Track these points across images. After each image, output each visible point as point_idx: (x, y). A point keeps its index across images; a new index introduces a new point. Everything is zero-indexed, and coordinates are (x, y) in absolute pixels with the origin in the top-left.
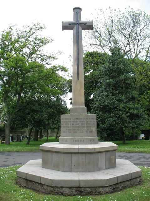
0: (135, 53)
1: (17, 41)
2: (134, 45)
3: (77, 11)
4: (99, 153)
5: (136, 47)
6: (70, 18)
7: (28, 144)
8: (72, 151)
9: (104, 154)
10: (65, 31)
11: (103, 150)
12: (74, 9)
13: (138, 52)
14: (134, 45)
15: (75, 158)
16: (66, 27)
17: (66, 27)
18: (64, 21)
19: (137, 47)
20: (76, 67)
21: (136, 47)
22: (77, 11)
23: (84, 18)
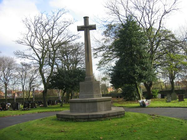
0: (149, 23)
1: (47, 24)
2: (149, 17)
3: (86, 19)
4: (101, 103)
5: (150, 19)
6: (82, 24)
7: (61, 106)
8: (85, 101)
9: (104, 102)
10: (83, 20)
11: (103, 100)
12: (84, 18)
13: (152, 23)
14: (149, 17)
15: (87, 105)
16: (80, 29)
17: (80, 29)
18: (79, 26)
19: (151, 19)
20: (87, 54)
21: (150, 19)
22: (86, 19)
23: (91, 23)
